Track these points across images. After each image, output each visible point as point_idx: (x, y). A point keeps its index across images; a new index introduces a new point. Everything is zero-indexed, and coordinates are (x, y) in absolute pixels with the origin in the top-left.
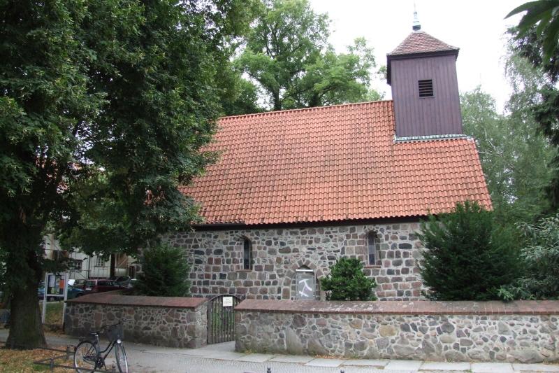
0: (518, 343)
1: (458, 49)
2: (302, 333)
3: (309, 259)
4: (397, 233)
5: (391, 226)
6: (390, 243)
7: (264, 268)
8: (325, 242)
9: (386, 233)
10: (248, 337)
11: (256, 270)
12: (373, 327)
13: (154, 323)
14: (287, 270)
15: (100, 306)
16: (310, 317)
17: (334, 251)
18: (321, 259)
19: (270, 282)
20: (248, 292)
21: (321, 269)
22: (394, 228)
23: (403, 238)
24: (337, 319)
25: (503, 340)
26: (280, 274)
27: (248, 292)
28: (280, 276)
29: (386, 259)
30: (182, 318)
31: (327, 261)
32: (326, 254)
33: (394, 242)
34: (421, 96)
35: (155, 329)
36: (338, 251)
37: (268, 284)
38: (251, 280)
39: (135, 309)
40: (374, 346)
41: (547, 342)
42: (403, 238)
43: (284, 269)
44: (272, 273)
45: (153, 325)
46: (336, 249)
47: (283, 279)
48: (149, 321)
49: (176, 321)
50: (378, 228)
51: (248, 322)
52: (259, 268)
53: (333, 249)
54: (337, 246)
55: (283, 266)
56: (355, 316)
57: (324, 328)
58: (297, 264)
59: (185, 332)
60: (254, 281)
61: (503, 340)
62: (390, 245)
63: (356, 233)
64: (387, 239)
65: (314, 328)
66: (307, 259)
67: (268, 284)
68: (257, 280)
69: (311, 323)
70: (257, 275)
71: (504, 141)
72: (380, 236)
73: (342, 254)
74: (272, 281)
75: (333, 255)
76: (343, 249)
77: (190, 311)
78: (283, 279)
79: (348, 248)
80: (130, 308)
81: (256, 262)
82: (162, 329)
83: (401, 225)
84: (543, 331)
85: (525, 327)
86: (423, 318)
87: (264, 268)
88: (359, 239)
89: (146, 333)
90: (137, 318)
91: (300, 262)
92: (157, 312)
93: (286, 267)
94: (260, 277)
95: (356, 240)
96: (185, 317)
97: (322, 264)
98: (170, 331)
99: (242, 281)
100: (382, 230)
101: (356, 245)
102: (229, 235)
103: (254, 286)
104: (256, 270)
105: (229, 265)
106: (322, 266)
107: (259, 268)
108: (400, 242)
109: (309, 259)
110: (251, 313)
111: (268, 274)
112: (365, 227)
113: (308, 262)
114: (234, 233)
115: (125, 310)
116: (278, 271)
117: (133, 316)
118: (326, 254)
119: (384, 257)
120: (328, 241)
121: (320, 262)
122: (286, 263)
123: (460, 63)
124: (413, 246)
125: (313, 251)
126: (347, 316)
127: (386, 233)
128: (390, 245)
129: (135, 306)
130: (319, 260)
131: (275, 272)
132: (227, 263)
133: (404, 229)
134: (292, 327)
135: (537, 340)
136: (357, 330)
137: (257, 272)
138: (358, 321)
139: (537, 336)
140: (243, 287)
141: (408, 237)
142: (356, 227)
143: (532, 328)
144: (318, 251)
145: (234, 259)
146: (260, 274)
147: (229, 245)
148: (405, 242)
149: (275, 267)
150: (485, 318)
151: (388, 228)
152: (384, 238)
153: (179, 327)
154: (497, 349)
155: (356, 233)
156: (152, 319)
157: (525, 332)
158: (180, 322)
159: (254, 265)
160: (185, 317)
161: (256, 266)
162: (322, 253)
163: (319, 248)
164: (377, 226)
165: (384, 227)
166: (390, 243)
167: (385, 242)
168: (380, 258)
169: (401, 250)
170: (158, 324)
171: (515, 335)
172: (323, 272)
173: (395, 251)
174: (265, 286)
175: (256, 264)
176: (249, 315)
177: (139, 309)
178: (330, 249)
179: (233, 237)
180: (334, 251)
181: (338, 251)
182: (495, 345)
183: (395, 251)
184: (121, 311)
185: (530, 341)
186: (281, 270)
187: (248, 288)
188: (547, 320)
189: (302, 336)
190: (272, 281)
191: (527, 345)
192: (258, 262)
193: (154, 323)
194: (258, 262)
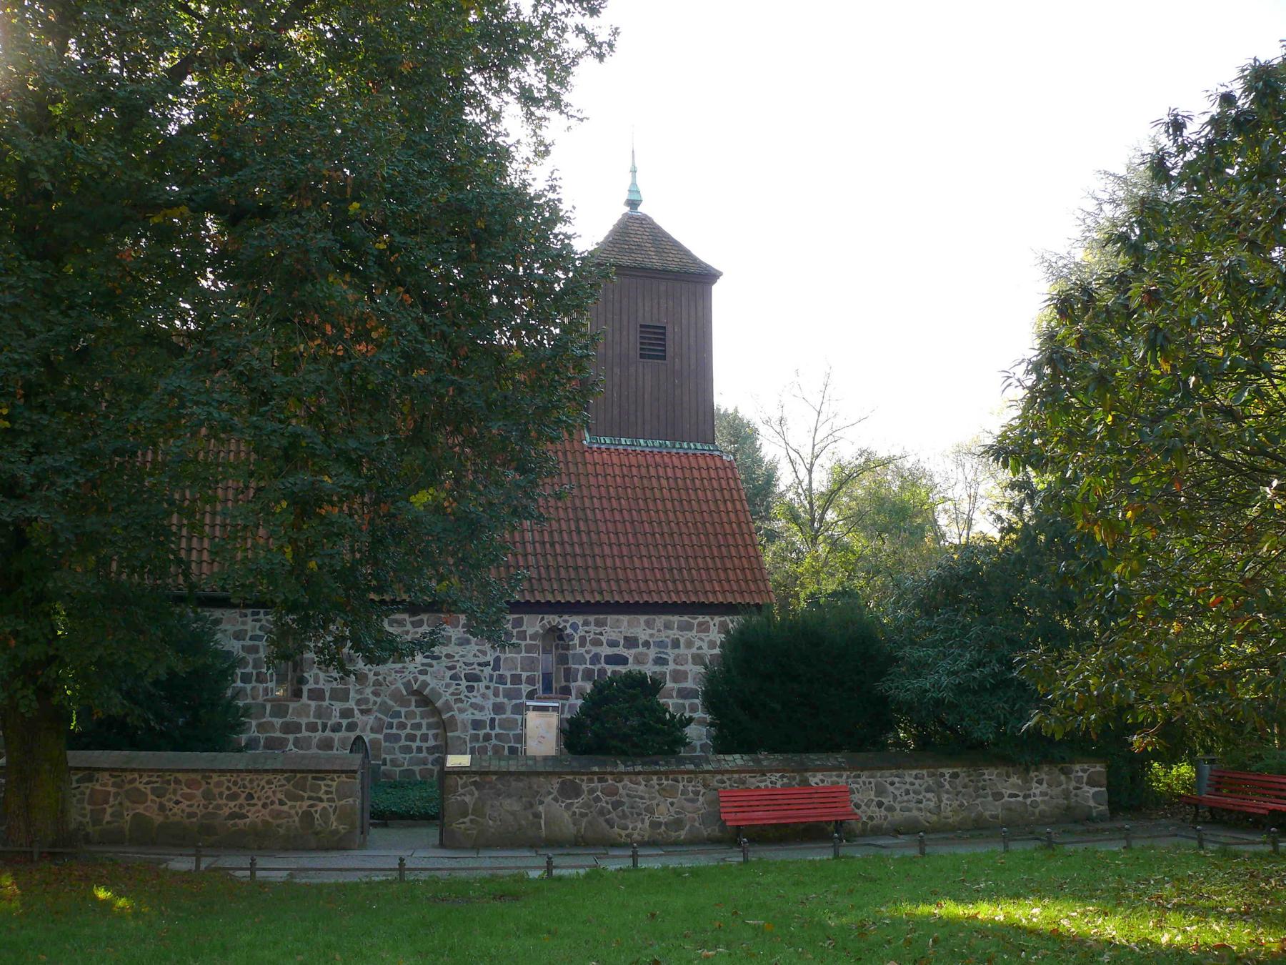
0: (898, 807)
1: (721, 274)
2: (574, 809)
3: (427, 678)
4: (601, 634)
5: (591, 618)
6: (587, 652)
7: (327, 695)
8: (460, 645)
9: (581, 632)
10: (471, 821)
11: (310, 698)
12: (697, 793)
13: (254, 805)
14: (379, 700)
15: (106, 775)
16: (591, 781)
17: (479, 664)
18: (451, 678)
19: (340, 725)
20: (291, 746)
21: (451, 699)
22: (598, 624)
23: (613, 644)
24: (639, 784)
25: (880, 805)
26: (363, 707)
27: (291, 746)
28: (362, 712)
29: (579, 683)
30: (327, 792)
31: (464, 683)
32: (462, 670)
33: (595, 650)
34: (642, 356)
35: (256, 815)
36: (487, 664)
37: (337, 728)
38: (296, 719)
39: (203, 777)
40: (697, 824)
41: (932, 804)
42: (613, 644)
43: (372, 698)
44: (347, 705)
45: (253, 809)
46: (482, 659)
47: (370, 720)
48: (242, 800)
49: (310, 798)
50: (567, 622)
51: (473, 794)
52: (317, 695)
53: (476, 660)
54: (484, 653)
55: (368, 691)
56: (667, 779)
57: (614, 799)
58: (402, 688)
59: (333, 818)
60: (304, 721)
61: (880, 805)
62: (588, 657)
63: (524, 628)
64: (582, 644)
65: (598, 799)
66: (422, 678)
67: (337, 728)
68: (312, 720)
69: (592, 791)
70: (313, 709)
71: (107, 51)
72: (571, 637)
73: (494, 669)
74: (345, 722)
75: (477, 672)
76: (497, 660)
77: (344, 778)
78: (370, 720)
79: (506, 659)
80: (193, 776)
81: (311, 681)
82: (278, 815)
83: (611, 618)
84: (928, 790)
85: (908, 786)
86: (773, 779)
87: (327, 695)
88: (528, 641)
89: (235, 825)
90: (208, 796)
91: (408, 685)
92: (263, 783)
93: (376, 694)
94: (319, 714)
95: (523, 643)
96: (333, 789)
97: (451, 690)
98: (297, 819)
99: (278, 722)
100: (574, 627)
101: (523, 654)
102: (250, 619)
103: (305, 734)
104: (310, 698)
105: (249, 687)
106: (453, 694)
107: (317, 695)
108: (606, 651)
109: (427, 678)
110: (477, 778)
111: (338, 706)
112: (543, 619)
113: (425, 684)
114: (261, 616)
115: (177, 781)
116: (358, 702)
117: (198, 793)
118: (462, 670)
119: (576, 681)
120: (468, 642)
121: (448, 686)
122: (377, 683)
123: (717, 290)
124: (631, 660)
125: (434, 662)
126: (655, 778)
127: (581, 632)
128: (588, 657)
129: (206, 773)
130: (448, 680)
131: (351, 704)
132: (243, 681)
133: (616, 625)
134: (556, 800)
135: (920, 802)
136: (670, 800)
137: (313, 704)
138: (672, 786)
139: (920, 797)
140: (278, 734)
141: (622, 642)
142: (526, 617)
143: (917, 786)
144: (445, 662)
145: (258, 674)
146: (319, 708)
147: (248, 643)
148: (615, 651)
149: (352, 694)
150: (859, 776)
151: (586, 623)
152: (577, 641)
153: (319, 809)
154: (871, 818)
155: (524, 628)
156: (250, 796)
157: (907, 792)
158: (321, 800)
159: (305, 688)
160: (333, 789)
161: (310, 690)
162: (454, 667)
163: (448, 656)
164: (566, 617)
165: (578, 620)
166: (587, 652)
167: (580, 650)
168: (567, 680)
169: (607, 667)
170: (265, 806)
171: (895, 797)
172: (455, 707)
173: (596, 668)
174: (328, 733)
175: (311, 685)
176: (475, 783)
177: (215, 778)
178: (471, 659)
179: (258, 624)
180: (479, 664)
181: (487, 664)
182: (869, 813)
183: (596, 668)
184: (168, 782)
185: (912, 805)
186: (366, 701)
187: (291, 737)
188: (934, 775)
189: (574, 813)
190: (345, 722)
191: (910, 810)
192: (316, 682)
193: (254, 805)
194: (316, 682)
